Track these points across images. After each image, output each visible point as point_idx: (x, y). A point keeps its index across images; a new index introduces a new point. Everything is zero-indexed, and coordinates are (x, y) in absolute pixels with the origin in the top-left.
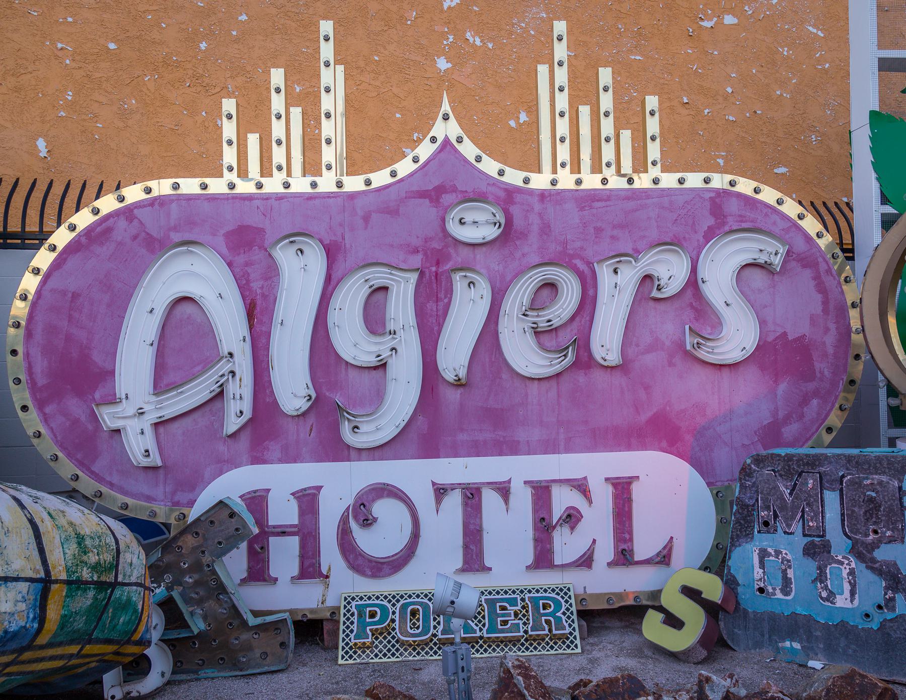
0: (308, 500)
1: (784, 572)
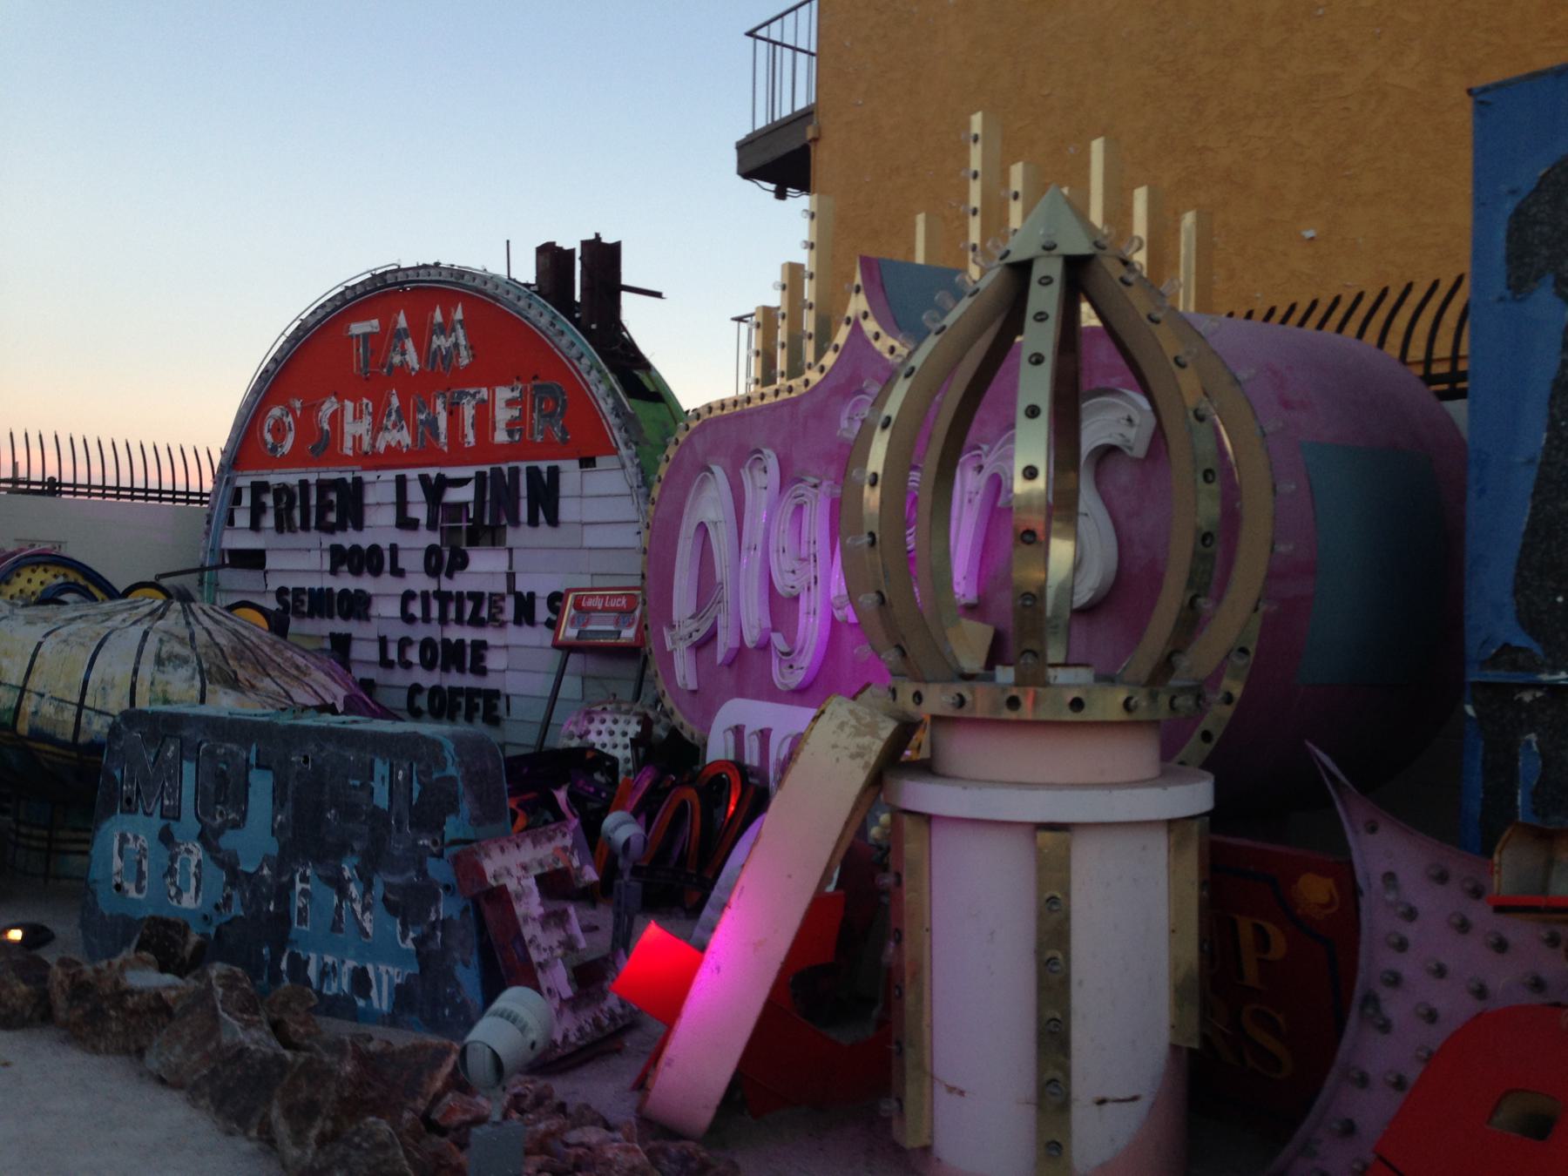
1: (140, 862)
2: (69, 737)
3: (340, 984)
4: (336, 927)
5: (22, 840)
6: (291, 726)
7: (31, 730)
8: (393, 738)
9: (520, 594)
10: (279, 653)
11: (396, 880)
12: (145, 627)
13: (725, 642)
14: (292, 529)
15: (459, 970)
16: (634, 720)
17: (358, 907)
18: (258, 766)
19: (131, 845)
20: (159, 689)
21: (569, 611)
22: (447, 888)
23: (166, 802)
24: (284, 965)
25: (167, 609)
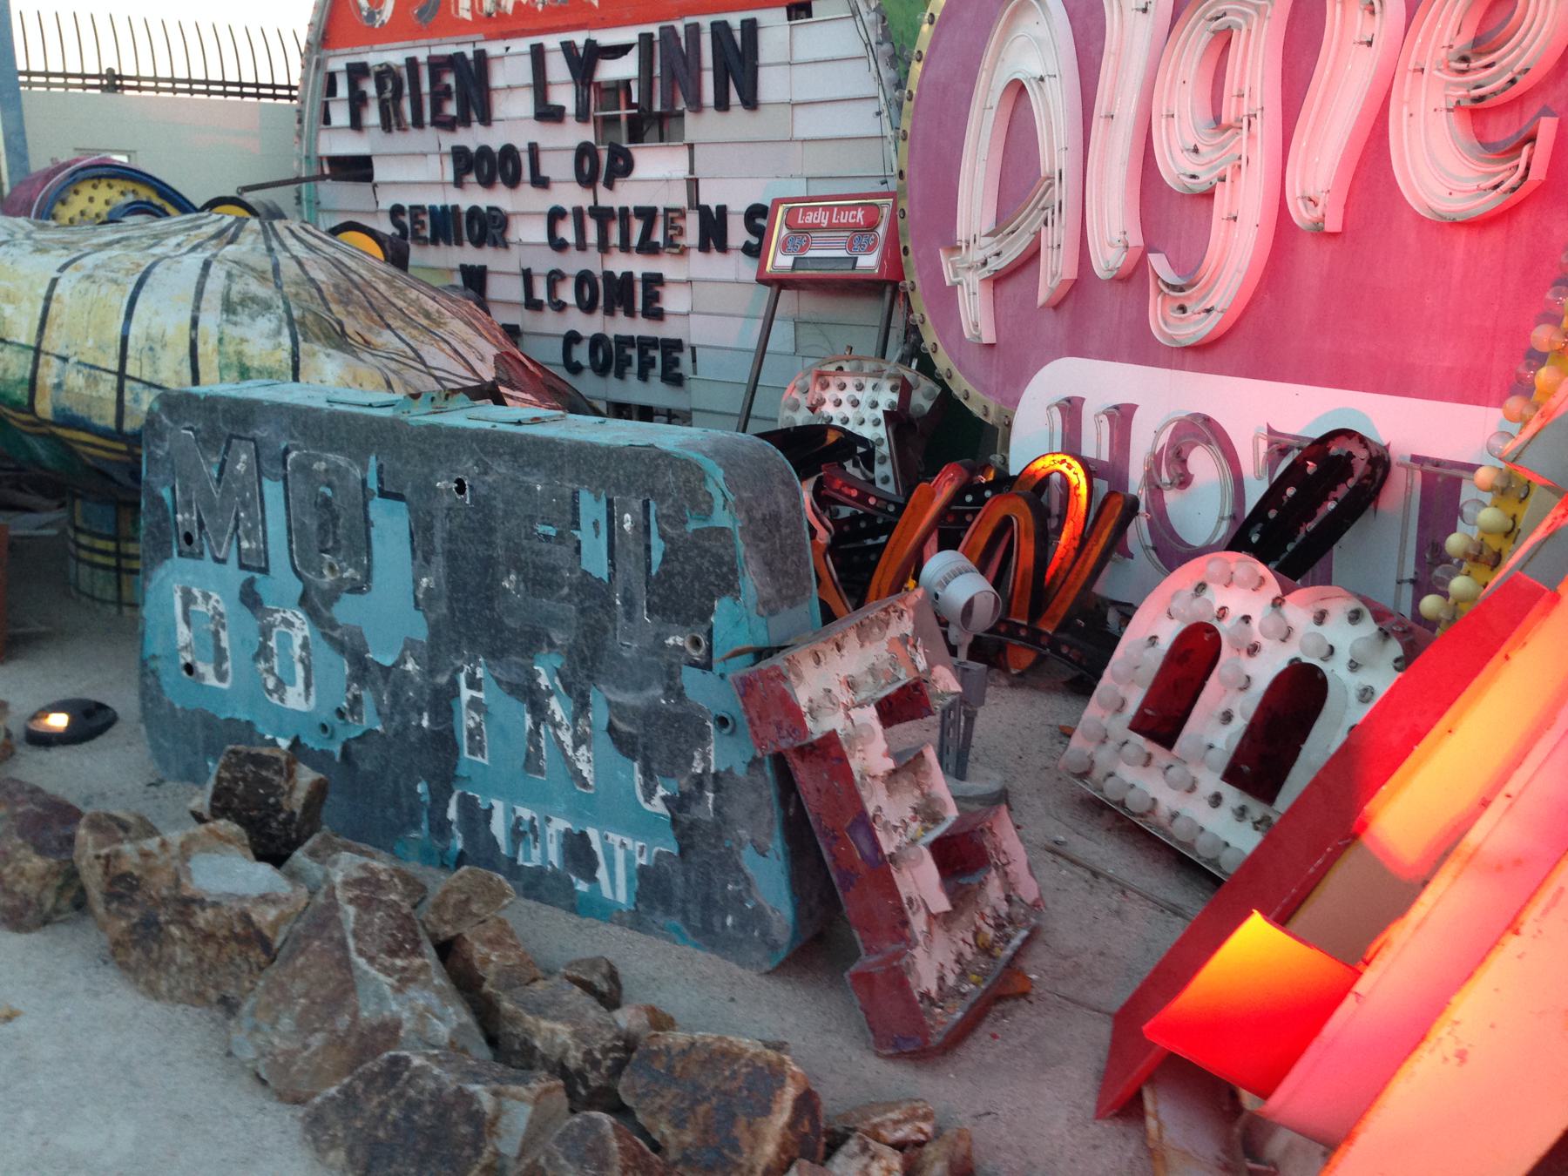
1: (216, 634)
2: (110, 422)
3: (545, 853)
4: (532, 762)
5: (84, 554)
6: (430, 427)
7: (55, 411)
8: (611, 454)
9: (707, 208)
10: (400, 292)
11: (628, 698)
12: (207, 254)
13: (1055, 269)
14: (401, 127)
15: (748, 859)
16: (887, 385)
17: (566, 737)
18: (383, 494)
19: (200, 607)
20: (230, 349)
21: (779, 231)
22: (722, 722)
23: (245, 545)
24: (452, 813)
25: (240, 229)
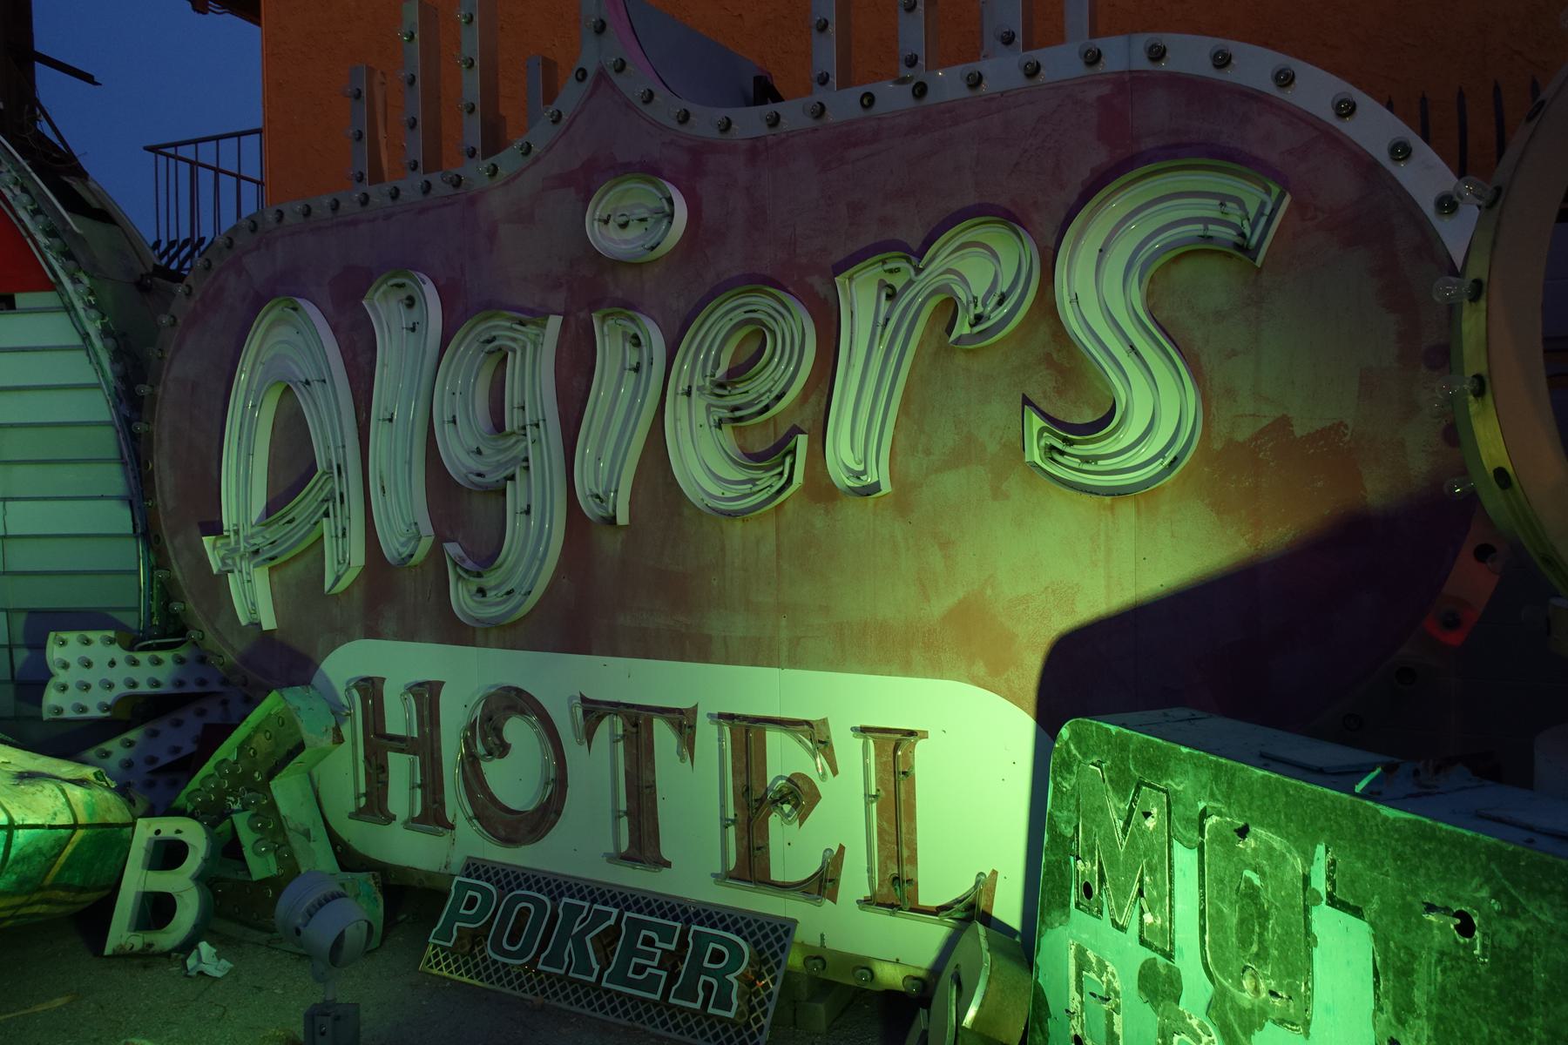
0: (427, 695)
